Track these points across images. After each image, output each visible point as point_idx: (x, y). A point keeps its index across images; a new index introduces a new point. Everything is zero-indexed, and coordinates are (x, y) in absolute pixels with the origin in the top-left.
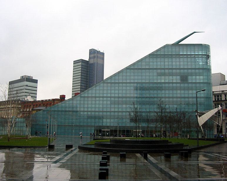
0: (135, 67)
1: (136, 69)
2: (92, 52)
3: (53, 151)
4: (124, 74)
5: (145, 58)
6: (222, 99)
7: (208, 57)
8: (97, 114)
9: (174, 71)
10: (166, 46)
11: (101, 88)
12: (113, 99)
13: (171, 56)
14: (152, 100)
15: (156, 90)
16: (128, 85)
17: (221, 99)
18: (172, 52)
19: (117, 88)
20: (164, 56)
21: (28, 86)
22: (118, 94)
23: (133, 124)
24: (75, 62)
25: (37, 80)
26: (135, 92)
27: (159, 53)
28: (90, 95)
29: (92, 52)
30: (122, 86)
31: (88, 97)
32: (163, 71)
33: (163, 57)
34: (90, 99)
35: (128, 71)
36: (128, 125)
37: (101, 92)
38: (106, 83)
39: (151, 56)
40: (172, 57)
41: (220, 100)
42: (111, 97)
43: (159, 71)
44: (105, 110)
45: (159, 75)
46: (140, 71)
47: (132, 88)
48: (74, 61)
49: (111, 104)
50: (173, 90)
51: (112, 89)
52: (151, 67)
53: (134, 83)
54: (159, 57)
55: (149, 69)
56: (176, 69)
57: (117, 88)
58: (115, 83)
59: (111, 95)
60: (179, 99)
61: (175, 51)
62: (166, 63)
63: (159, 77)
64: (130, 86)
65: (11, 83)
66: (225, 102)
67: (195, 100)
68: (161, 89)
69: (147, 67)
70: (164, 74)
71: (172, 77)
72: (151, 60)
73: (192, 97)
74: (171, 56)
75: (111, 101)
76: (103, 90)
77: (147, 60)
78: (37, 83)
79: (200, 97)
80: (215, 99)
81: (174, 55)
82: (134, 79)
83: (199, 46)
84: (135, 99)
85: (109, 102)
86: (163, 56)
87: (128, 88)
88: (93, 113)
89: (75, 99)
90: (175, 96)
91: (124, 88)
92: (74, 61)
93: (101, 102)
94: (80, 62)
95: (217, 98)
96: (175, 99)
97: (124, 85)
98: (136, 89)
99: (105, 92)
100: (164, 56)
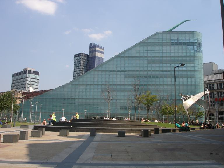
0: (104, 69)
1: (127, 57)
2: (93, 47)
3: (27, 133)
4: (115, 62)
6: (215, 88)
8: (88, 101)
9: (165, 59)
10: (157, 34)
11: (92, 76)
12: (103, 87)
13: (162, 44)
14: (158, 87)
15: (162, 77)
17: (213, 88)
19: (107, 76)
20: (155, 44)
21: (30, 78)
23: (122, 112)
24: (76, 56)
25: (39, 72)
27: (149, 41)
28: (81, 83)
29: (93, 47)
31: (79, 85)
32: (153, 59)
33: (153, 45)
34: (96, 86)
35: (118, 59)
39: (141, 44)
41: (212, 89)
42: (102, 85)
43: (149, 59)
44: (96, 97)
46: (131, 59)
50: (187, 78)
52: (142, 55)
54: (158, 45)
56: (166, 57)
57: (115, 76)
58: (106, 71)
60: (185, 87)
62: (180, 51)
63: (149, 65)
65: (14, 75)
66: (217, 91)
67: (173, 87)
68: (156, 77)
69: (138, 55)
70: (154, 62)
72: (142, 48)
73: (190, 85)
76: (102, 78)
77: (138, 48)
78: (39, 75)
79: (179, 85)
80: (218, 87)
82: (124, 67)
85: (100, 90)
86: (162, 44)
88: (84, 101)
90: (165, 83)
95: (220, 87)
96: (165, 87)
99: (96, 79)
100: (155, 44)
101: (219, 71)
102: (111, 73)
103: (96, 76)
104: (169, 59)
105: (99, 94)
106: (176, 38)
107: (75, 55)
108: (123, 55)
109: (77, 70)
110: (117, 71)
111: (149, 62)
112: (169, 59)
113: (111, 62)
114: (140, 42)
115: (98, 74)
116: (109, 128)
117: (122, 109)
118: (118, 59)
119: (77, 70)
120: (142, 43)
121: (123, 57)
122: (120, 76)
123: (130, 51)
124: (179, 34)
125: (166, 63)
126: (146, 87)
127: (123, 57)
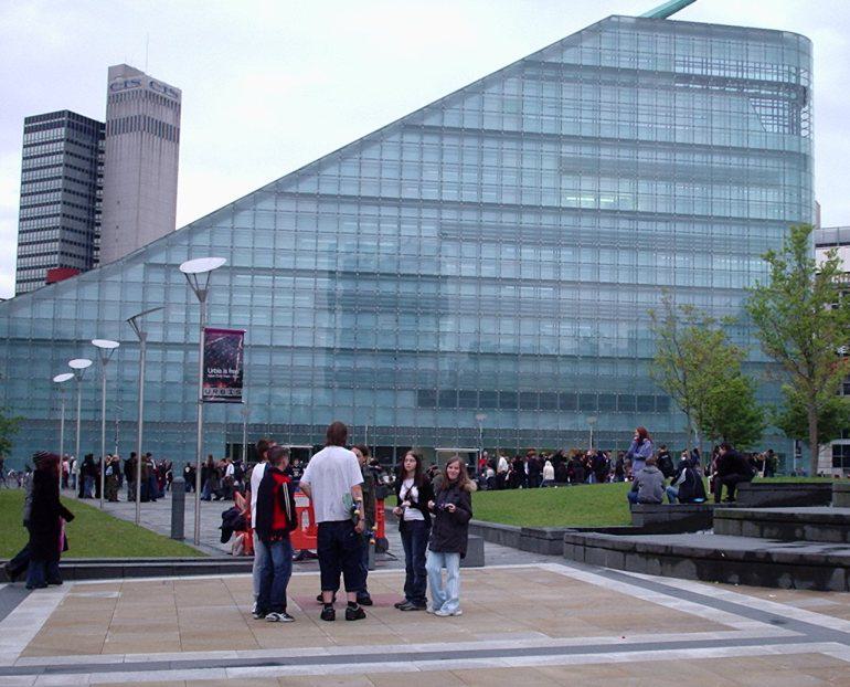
0: (328, 189)
2: (126, 85)
5: (501, 76)
7: (800, 96)
13: (632, 78)
16: (285, 281)
18: (400, 187)
22: (480, 188)
24: (34, 124)
26: (325, 320)
27: (569, 57)
29: (126, 85)
30: (253, 290)
35: (411, 138)
36: (406, 421)
37: (264, 242)
38: (291, 194)
39: (528, 72)
40: (632, 85)
45: (568, 172)
47: (306, 301)
48: (28, 120)
49: (443, 236)
51: (279, 246)
53: (315, 273)
55: (519, 136)
59: (187, 333)
61: (651, 54)
63: (568, 182)
64: (295, 291)
69: (510, 126)
71: (513, 250)
72: (531, 90)
74: (632, 78)
75: (440, 224)
76: (275, 234)
77: (511, 88)
81: (646, 73)
83: (767, 40)
84: (322, 361)
87: (284, 299)
89: (118, 278)
91: (263, 299)
92: (28, 120)
93: (263, 299)
94: (59, 125)
97: (264, 280)
98: (332, 303)
99: (286, 243)
101: (838, 231)
102: (371, 211)
103: (287, 224)
104: (662, 157)
105: (305, 321)
106: (690, 59)
107: (168, 99)
108: (432, 121)
109: (36, 211)
110: (399, 203)
111: (568, 168)
112: (662, 157)
113: (372, 153)
114: (523, 59)
115: (297, 217)
116: (511, 566)
117: (426, 399)
118: (408, 138)
119: (36, 211)
120: (536, 67)
121: (440, 131)
122: (211, 240)
123: (472, 103)
124: (717, 35)
125: (649, 177)
126: (429, 289)
127: (440, 131)
